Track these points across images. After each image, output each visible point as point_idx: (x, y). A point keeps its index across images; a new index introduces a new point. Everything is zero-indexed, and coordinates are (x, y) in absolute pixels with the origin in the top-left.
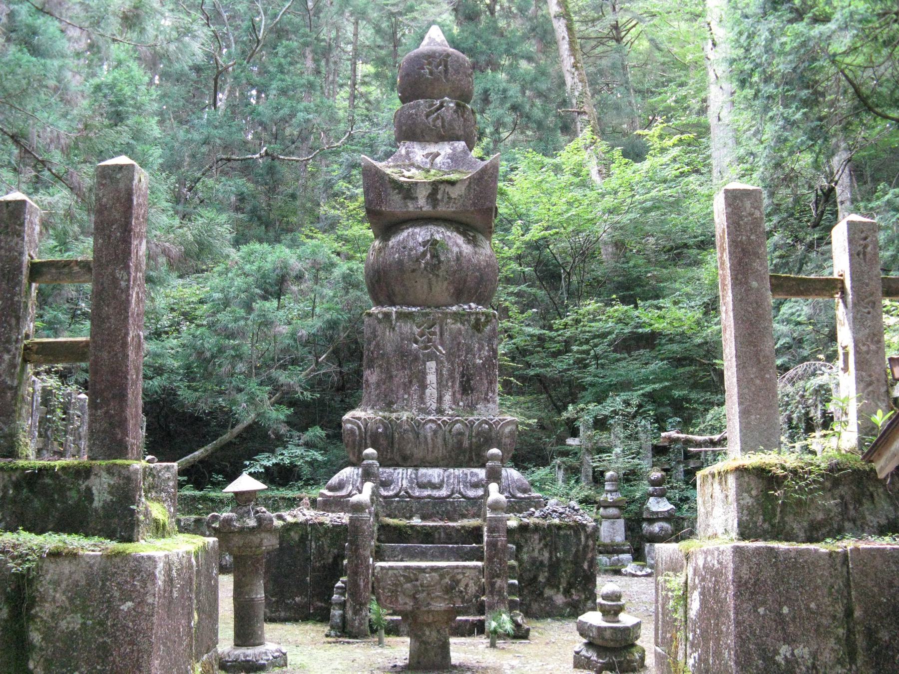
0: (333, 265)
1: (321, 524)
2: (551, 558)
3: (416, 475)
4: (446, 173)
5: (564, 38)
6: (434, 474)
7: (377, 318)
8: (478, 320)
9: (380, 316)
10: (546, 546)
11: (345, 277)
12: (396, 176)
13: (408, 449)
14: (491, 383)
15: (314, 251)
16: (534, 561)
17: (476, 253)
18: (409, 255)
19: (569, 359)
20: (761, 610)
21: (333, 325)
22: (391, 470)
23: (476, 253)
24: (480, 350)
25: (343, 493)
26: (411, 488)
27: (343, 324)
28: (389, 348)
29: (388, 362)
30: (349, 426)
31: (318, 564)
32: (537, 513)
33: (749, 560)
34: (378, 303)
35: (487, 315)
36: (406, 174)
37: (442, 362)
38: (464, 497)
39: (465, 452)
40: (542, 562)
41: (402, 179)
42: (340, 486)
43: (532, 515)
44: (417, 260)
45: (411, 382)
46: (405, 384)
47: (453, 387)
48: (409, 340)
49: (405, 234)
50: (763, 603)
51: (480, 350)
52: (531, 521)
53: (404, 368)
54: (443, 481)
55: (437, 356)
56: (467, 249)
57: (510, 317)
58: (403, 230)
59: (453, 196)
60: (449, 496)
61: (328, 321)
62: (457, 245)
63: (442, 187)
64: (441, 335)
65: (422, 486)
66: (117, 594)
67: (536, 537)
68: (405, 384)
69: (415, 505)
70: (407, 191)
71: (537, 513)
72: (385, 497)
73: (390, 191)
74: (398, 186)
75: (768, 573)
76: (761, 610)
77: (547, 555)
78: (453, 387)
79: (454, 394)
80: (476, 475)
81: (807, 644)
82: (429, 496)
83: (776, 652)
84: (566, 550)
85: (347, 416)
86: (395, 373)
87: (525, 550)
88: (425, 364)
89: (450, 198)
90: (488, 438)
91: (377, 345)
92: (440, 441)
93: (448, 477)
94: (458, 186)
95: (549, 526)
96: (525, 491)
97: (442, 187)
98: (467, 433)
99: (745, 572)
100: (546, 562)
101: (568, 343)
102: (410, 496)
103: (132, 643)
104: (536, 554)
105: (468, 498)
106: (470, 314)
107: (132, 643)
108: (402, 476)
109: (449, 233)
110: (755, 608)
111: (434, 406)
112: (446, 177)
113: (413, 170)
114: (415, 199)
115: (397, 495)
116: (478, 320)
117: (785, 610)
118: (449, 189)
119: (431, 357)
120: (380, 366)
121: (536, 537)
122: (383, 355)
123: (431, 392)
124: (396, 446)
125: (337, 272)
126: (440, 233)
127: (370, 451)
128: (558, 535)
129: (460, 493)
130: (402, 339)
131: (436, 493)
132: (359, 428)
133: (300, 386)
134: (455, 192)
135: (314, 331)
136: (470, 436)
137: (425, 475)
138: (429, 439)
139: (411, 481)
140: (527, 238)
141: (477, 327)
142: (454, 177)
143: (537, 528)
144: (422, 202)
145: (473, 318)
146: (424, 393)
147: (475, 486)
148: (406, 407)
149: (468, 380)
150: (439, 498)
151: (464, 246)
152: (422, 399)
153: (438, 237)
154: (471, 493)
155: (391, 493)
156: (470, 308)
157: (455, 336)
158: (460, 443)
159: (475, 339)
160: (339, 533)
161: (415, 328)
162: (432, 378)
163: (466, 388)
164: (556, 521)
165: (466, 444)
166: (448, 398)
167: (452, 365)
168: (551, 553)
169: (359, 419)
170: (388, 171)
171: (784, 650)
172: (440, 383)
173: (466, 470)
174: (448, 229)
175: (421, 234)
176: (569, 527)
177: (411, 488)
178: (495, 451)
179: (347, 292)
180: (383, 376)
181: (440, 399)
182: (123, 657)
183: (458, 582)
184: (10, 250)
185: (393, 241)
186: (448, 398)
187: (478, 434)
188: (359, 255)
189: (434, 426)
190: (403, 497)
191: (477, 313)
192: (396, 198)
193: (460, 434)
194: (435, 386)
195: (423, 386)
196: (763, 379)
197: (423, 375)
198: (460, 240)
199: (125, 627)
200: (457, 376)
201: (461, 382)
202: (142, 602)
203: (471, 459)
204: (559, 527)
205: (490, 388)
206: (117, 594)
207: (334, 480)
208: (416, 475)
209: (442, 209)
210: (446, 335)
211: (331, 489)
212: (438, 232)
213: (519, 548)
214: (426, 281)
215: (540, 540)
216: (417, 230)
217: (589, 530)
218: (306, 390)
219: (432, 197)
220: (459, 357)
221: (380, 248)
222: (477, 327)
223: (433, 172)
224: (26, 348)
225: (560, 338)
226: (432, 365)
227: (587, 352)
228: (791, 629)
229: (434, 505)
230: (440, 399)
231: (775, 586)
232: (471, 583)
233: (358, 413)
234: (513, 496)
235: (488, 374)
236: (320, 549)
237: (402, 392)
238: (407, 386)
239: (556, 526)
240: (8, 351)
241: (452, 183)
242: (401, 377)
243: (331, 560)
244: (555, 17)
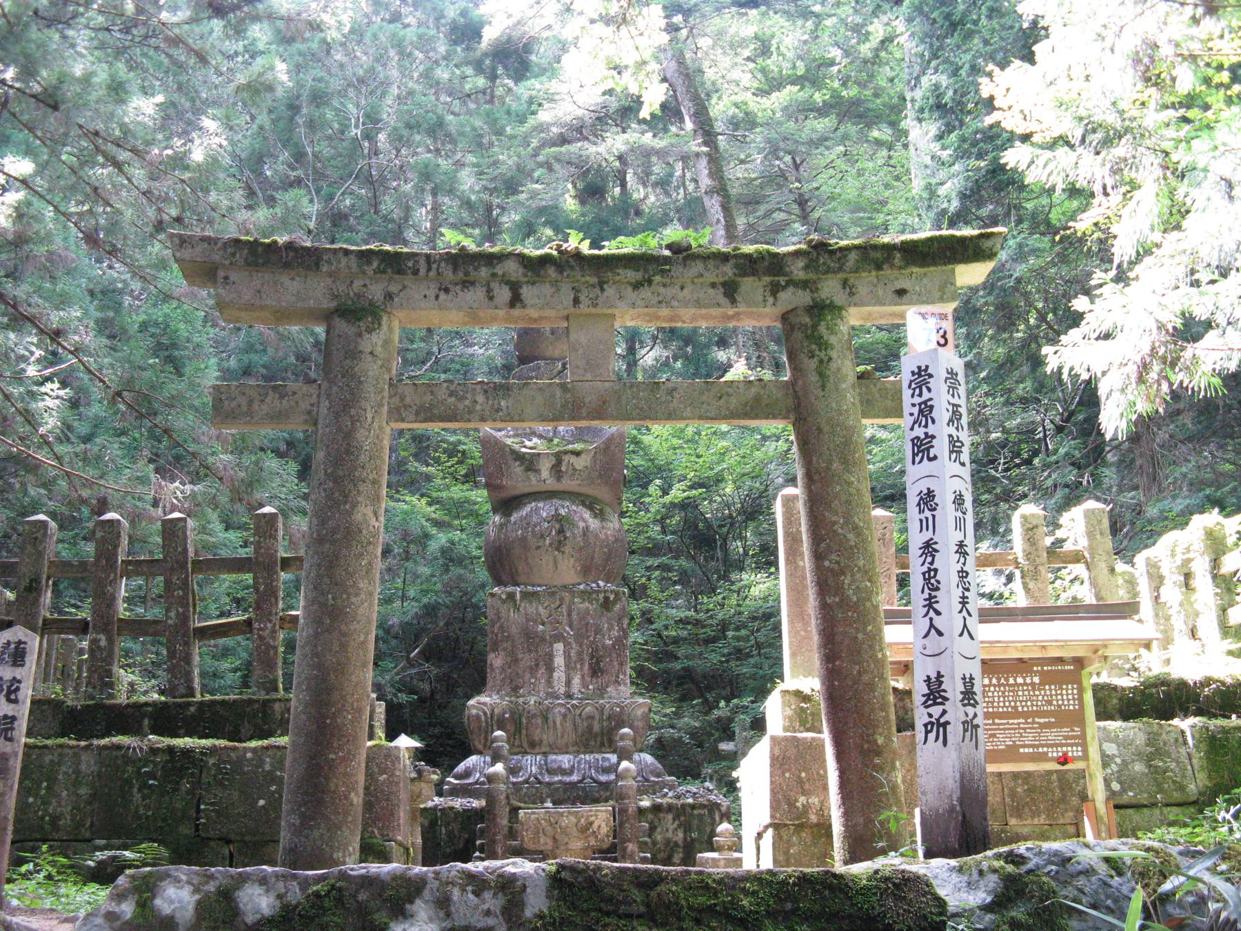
0: (427, 536)
1: (452, 808)
2: (685, 839)
3: (546, 761)
4: (570, 443)
5: (718, 221)
6: (565, 760)
7: (500, 598)
8: (606, 598)
9: (504, 597)
10: (679, 826)
11: (443, 551)
12: (516, 447)
13: (537, 734)
14: (621, 664)
15: (404, 519)
16: (667, 842)
17: (603, 527)
18: (533, 531)
19: (724, 648)
20: (787, 775)
21: (430, 611)
22: (519, 757)
23: (603, 527)
24: (609, 630)
25: (471, 780)
26: (541, 774)
27: (444, 610)
28: (514, 630)
29: (513, 646)
30: (474, 712)
31: (448, 850)
32: (670, 794)
33: (779, 744)
34: (499, 582)
35: (617, 594)
36: (527, 443)
37: (569, 644)
38: (595, 781)
39: (596, 736)
40: (676, 844)
41: (524, 450)
42: (467, 773)
43: (665, 795)
44: (542, 536)
45: (537, 665)
46: (531, 668)
47: (582, 669)
48: (535, 621)
49: (528, 509)
50: (789, 770)
51: (609, 630)
52: (664, 801)
53: (530, 651)
54: (573, 766)
55: (564, 638)
56: (594, 524)
57: (648, 596)
58: (525, 505)
59: (578, 467)
60: (580, 782)
61: (425, 606)
62: (584, 520)
63: (566, 458)
64: (569, 615)
65: (551, 772)
66: (376, 770)
67: (670, 817)
68: (531, 668)
69: (545, 790)
70: (529, 463)
71: (670, 794)
72: (514, 784)
73: (511, 462)
74: (519, 457)
75: (792, 752)
76: (787, 775)
77: (681, 835)
78: (582, 669)
79: (583, 676)
80: (608, 759)
81: (818, 796)
82: (560, 782)
83: (796, 801)
84: (699, 830)
85: (471, 702)
86: (520, 656)
87: (659, 830)
88: (551, 646)
89: (575, 470)
90: (619, 720)
91: (502, 627)
92: (569, 725)
93: (579, 762)
94: (583, 456)
95: (683, 806)
96: (658, 776)
97: (566, 458)
98: (597, 717)
99: (777, 752)
100: (680, 843)
101: (724, 626)
102: (540, 782)
103: (387, 800)
104: (670, 834)
105: (600, 783)
106: (598, 592)
107: (387, 800)
108: (531, 764)
109: (574, 508)
110: (783, 774)
111: (562, 690)
112: (570, 447)
113: (535, 440)
114: (538, 471)
115: (526, 781)
116: (606, 598)
117: (803, 775)
118: (573, 459)
119: (559, 637)
120: (505, 650)
121: (670, 817)
122: (508, 637)
123: (559, 675)
124: (524, 732)
125: (433, 546)
126: (565, 508)
127: (499, 733)
128: (692, 815)
129: (592, 778)
130: (528, 620)
131: (567, 779)
132: (485, 714)
133: (392, 686)
134: (580, 463)
135: (408, 618)
136: (601, 720)
137: (555, 761)
138: (558, 723)
139: (540, 767)
140: (667, 499)
141: (607, 605)
142: (578, 447)
143: (670, 808)
144: (545, 474)
145: (601, 596)
146: (551, 677)
147: (607, 771)
148: (534, 690)
149: (598, 663)
150: (570, 783)
151: (591, 520)
152: (549, 682)
153: (563, 512)
154: (603, 778)
155: (520, 779)
156: (598, 586)
157: (584, 616)
158: (590, 728)
159: (604, 620)
160: (469, 818)
161: (540, 608)
162: (559, 661)
163: (596, 670)
164: (690, 801)
165: (596, 727)
166: (576, 681)
167: (581, 646)
168: (685, 832)
169: (485, 704)
170: (509, 441)
171: (802, 799)
172: (567, 666)
173: (597, 756)
174: (573, 503)
175: (546, 509)
176: (702, 806)
177: (541, 774)
178: (626, 730)
179: (447, 570)
180: (509, 659)
181: (568, 683)
182: (382, 808)
183: (591, 823)
184: (268, 548)
185: (515, 517)
186: (576, 681)
187: (609, 718)
188: (456, 522)
189: (563, 710)
190: (532, 783)
191: (606, 592)
192: (517, 469)
193: (591, 717)
194: (563, 669)
195: (550, 669)
196: (806, 631)
197: (550, 656)
198: (587, 515)
199: (382, 791)
200: (586, 658)
201: (590, 665)
202: (393, 775)
203: (602, 744)
204: (693, 807)
205: (621, 670)
206: (376, 770)
207: (461, 767)
208: (546, 761)
209: (567, 484)
210: (574, 616)
211: (456, 777)
212: (563, 507)
213: (653, 828)
214: (551, 559)
215: (674, 820)
216: (541, 505)
217: (723, 809)
218: (400, 691)
219: (557, 470)
220: (588, 637)
221: (501, 525)
222: (607, 605)
223: (556, 441)
224: (282, 619)
225: (710, 621)
226: (559, 647)
227: (747, 639)
228: (807, 786)
229: (565, 791)
230: (568, 683)
231: (796, 760)
232: (603, 825)
233: (483, 698)
234: (647, 780)
235: (619, 655)
236: (450, 834)
237: (528, 676)
238: (533, 670)
239: (689, 805)
240: (270, 621)
241: (577, 454)
242: (526, 660)
243: (461, 846)
244: (706, 193)
